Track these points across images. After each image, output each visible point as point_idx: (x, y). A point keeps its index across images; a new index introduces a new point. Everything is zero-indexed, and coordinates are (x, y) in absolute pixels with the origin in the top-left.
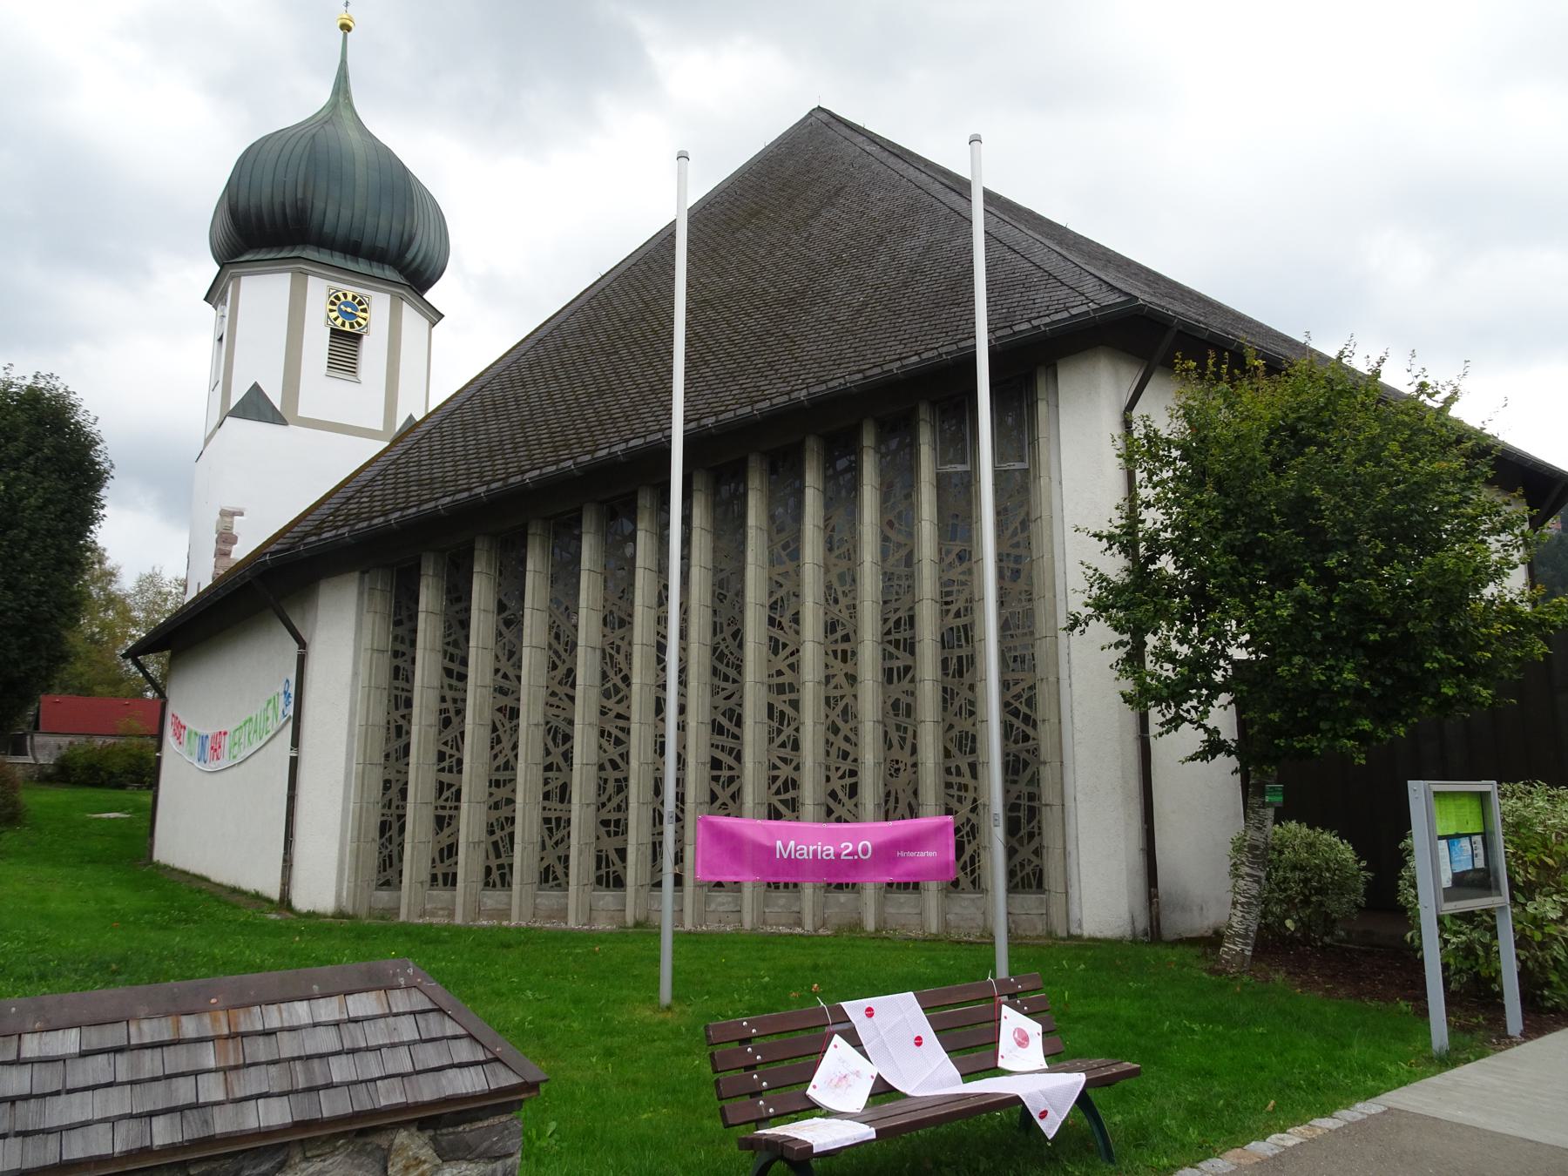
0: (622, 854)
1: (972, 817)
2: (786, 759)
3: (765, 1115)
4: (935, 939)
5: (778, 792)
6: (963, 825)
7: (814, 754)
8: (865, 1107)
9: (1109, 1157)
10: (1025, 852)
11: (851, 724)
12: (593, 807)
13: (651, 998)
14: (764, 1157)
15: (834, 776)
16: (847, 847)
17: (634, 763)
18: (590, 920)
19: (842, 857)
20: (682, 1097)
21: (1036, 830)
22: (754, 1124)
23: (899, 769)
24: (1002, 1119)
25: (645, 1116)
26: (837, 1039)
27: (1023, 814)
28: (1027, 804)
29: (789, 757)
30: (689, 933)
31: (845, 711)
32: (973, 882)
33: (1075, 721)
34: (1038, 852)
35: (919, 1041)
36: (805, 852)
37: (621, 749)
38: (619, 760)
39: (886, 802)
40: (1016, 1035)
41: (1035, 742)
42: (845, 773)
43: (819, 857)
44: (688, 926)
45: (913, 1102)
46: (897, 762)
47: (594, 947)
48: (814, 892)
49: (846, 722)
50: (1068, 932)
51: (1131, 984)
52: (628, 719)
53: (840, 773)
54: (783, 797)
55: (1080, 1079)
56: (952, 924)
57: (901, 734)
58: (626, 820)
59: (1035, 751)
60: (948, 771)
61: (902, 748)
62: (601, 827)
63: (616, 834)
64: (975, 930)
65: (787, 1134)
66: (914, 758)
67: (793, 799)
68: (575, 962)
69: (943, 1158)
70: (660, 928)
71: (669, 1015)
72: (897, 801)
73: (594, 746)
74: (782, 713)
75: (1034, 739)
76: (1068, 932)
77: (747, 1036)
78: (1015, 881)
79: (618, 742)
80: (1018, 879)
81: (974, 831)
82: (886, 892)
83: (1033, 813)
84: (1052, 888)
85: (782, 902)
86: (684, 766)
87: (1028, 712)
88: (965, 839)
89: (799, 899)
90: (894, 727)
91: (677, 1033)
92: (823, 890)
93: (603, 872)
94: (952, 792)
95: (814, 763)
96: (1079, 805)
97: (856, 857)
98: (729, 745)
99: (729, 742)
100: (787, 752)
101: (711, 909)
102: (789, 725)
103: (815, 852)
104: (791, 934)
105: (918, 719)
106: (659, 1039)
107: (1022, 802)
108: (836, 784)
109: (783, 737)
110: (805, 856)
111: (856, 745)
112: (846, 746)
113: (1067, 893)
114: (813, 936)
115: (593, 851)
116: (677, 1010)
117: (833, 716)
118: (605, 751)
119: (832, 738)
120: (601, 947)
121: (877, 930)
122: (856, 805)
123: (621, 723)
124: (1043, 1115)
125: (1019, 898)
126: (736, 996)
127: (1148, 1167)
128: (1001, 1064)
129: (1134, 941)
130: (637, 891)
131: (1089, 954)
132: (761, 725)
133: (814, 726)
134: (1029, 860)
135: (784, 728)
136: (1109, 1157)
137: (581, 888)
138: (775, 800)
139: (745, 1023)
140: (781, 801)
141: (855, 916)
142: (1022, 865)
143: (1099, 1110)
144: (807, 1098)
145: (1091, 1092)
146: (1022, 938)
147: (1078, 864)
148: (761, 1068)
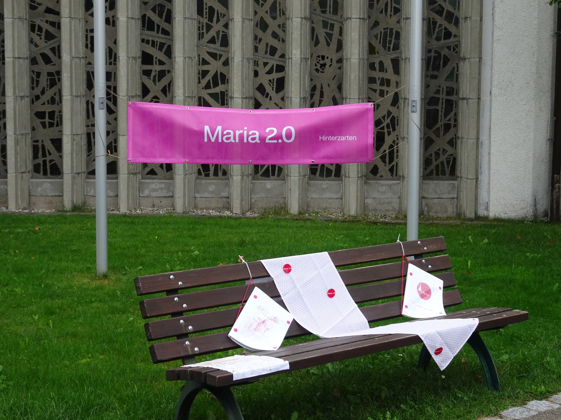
0: (58, 143)
1: (393, 110)
2: (216, 54)
3: (190, 353)
4: (354, 221)
5: (207, 86)
6: (384, 117)
7: (243, 49)
8: (281, 347)
9: (495, 385)
10: (441, 143)
11: (279, 21)
12: (27, 100)
13: (89, 268)
14: (192, 386)
15: (262, 71)
16: (272, 132)
17: (66, 57)
18: (30, 204)
19: (267, 141)
20: (117, 346)
21: (452, 122)
22: (176, 337)
23: (324, 65)
24: (404, 359)
25: (84, 360)
26: (257, 291)
27: (441, 107)
28: (445, 97)
29: (218, 53)
30: (125, 216)
31: (273, 8)
32: (391, 170)
33: (496, 18)
34: (452, 143)
35: (331, 294)
36: (232, 136)
37: (52, 43)
38: (50, 54)
39: (312, 96)
40: (420, 289)
41: (457, 39)
42: (272, 68)
43: (245, 141)
44: (123, 209)
45: (325, 341)
46: (323, 58)
47: (35, 227)
48: (242, 179)
49: (274, 18)
50: (476, 213)
51: (528, 254)
52: (58, 13)
53: (268, 68)
54: (213, 91)
55: (473, 323)
56: (371, 207)
57: (328, 31)
58: (60, 112)
59: (456, 48)
60: (372, 66)
61: (328, 44)
62: (36, 118)
63: (51, 125)
64: (390, 212)
65: (210, 366)
66: (339, 55)
67: (223, 93)
68: (16, 239)
69: (350, 388)
70: (95, 210)
71: (106, 282)
72: (322, 95)
73: (25, 40)
74: (211, 10)
75: (455, 36)
76: (476, 213)
77: (178, 309)
78: (429, 170)
79: (49, 36)
80: (433, 167)
81: (394, 123)
82: (310, 179)
83: (450, 106)
84: (464, 175)
85: (212, 188)
86: (115, 60)
87: (451, 9)
88: (386, 130)
89: (228, 185)
90: (321, 23)
91: (113, 296)
92: (250, 177)
93: (40, 160)
94: (374, 86)
95: (243, 58)
96: (493, 98)
97: (280, 141)
98: (159, 40)
99: (160, 38)
100: (216, 48)
101: (145, 195)
102: (218, 20)
103: (241, 136)
104: (220, 217)
105: (345, 16)
106: (96, 301)
107: (440, 96)
108: (264, 79)
109: (212, 33)
110: (232, 140)
111: (283, 41)
112: (274, 43)
113: (477, 179)
114: (240, 218)
115: (29, 141)
116: (113, 278)
117: (262, 13)
118: (36, 46)
119: (260, 34)
120: (41, 227)
121: (300, 213)
122: (283, 99)
123: (51, 18)
124: (439, 351)
125: (432, 184)
126: (168, 266)
127: (527, 393)
128: (405, 312)
129: (535, 220)
130: (73, 178)
131: (493, 231)
132: (190, 21)
133: (243, 22)
134: (444, 150)
135: (214, 24)
136: (495, 385)
137: (19, 176)
138: (205, 94)
139: (172, 277)
140: (211, 95)
141: (281, 201)
142: (437, 154)
143: (490, 351)
144: (229, 339)
145: (481, 334)
146: (433, 219)
147: (489, 154)
148: (185, 315)
